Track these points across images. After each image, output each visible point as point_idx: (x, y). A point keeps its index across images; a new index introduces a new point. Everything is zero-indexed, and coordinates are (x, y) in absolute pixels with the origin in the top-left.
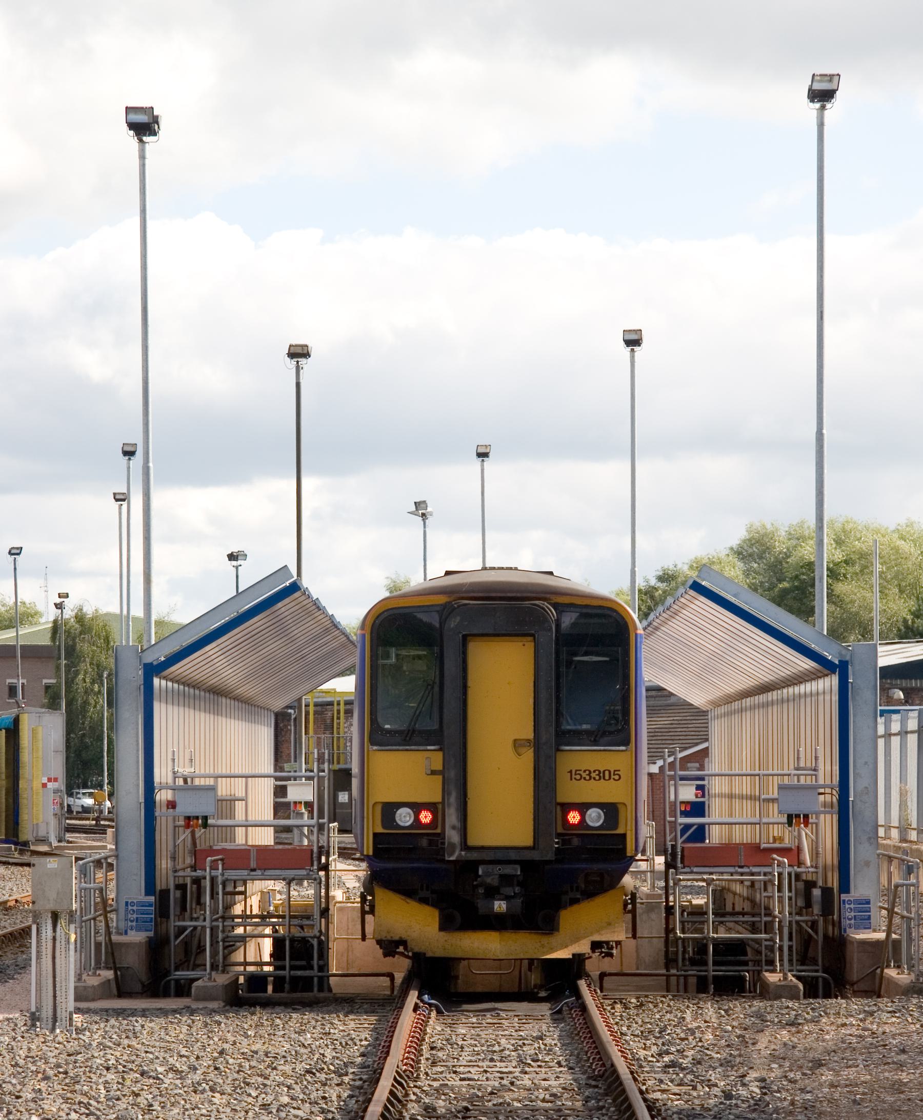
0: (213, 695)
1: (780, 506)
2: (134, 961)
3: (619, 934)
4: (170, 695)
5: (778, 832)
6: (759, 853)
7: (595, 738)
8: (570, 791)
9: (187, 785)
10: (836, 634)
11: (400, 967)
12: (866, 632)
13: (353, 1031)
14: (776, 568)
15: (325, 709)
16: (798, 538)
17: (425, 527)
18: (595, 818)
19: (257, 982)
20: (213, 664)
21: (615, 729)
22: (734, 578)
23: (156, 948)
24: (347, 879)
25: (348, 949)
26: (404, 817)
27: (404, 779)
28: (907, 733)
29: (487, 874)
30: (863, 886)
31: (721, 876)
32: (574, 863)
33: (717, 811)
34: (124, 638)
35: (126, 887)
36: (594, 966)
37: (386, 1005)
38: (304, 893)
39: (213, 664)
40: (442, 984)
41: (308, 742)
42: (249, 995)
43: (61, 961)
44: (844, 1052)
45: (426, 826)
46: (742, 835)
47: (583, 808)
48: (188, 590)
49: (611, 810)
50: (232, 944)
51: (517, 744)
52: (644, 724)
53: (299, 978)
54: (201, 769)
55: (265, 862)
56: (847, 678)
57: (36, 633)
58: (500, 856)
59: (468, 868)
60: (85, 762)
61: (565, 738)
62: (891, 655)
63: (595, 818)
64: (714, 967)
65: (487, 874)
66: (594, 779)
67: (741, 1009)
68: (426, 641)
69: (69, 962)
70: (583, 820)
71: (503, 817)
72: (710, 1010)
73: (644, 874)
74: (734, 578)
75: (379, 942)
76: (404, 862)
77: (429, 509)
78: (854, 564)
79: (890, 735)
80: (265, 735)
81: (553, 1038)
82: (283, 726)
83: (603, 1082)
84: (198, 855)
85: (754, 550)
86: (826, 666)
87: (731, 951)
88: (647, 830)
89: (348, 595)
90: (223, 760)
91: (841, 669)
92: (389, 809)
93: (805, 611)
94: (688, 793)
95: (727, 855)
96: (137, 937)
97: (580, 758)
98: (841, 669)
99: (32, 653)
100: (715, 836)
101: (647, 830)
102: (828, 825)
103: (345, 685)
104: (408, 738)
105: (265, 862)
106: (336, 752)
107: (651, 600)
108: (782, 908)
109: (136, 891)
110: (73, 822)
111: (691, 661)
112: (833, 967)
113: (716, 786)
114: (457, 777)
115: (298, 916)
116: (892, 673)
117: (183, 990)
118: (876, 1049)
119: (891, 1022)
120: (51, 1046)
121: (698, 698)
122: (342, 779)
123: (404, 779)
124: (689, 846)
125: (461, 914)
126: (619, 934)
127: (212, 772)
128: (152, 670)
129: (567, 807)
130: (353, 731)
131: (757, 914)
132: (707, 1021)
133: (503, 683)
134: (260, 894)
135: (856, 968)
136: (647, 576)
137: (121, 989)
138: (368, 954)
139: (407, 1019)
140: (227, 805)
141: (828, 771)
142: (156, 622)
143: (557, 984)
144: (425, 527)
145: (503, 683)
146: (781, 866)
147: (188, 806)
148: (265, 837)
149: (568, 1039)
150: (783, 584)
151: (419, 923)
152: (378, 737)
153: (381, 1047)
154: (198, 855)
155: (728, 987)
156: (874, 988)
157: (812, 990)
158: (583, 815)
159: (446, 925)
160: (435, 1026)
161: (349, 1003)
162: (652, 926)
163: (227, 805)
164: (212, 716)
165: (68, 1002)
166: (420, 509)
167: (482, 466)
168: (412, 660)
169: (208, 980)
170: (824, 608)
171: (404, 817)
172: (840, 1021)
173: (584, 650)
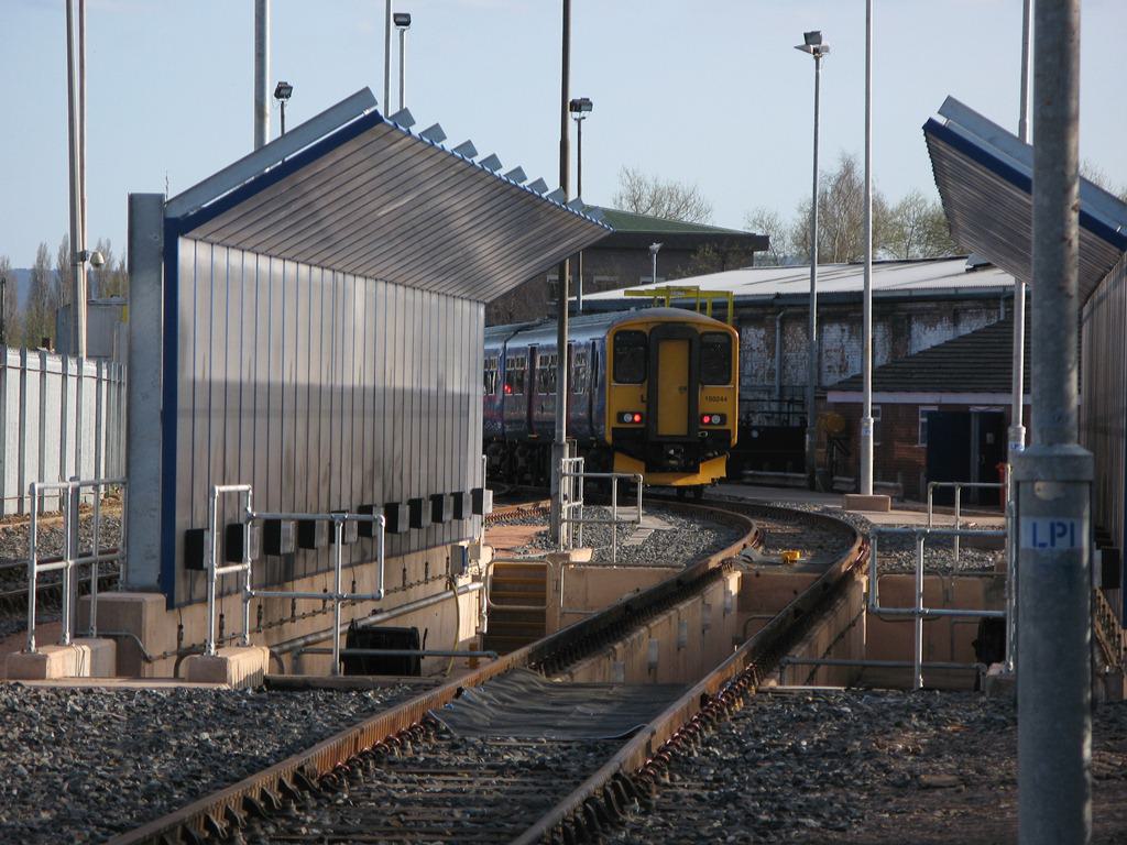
4: (303, 291)
8: (705, 406)
17: (817, 68)
45: (637, 423)
47: (711, 416)
51: (680, 389)
56: (1113, 231)
63: (716, 419)
70: (710, 420)
71: (672, 422)
75: (955, 325)
77: (823, 43)
114: (651, 402)
127: (450, 304)
129: (703, 415)
133: (673, 364)
142: (293, 673)
144: (817, 68)
145: (673, 364)
158: (711, 418)
164: (380, 385)
166: (812, 38)
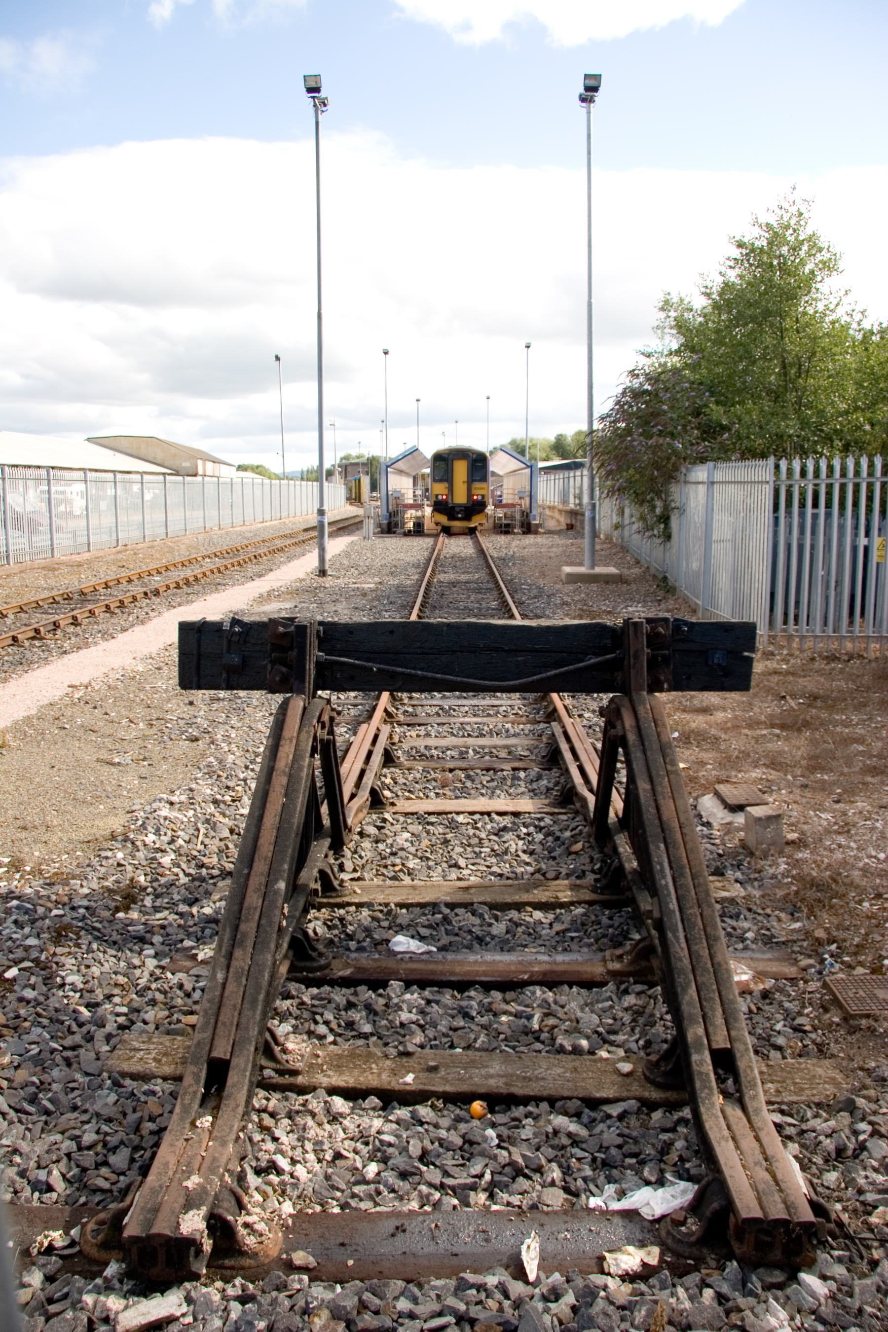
0: (401, 472)
1: (519, 434)
2: (385, 527)
3: (484, 521)
5: (517, 501)
6: (513, 505)
7: (480, 481)
8: (474, 492)
9: (395, 491)
10: (530, 460)
11: (439, 528)
12: (536, 460)
13: (430, 541)
14: (518, 447)
15: (423, 475)
16: (522, 440)
18: (480, 498)
19: (410, 531)
20: (400, 465)
21: (484, 479)
22: (509, 448)
23: (389, 524)
24: (428, 511)
25: (428, 525)
26: (440, 497)
27: (440, 489)
28: (713, 483)
29: (457, 509)
30: (534, 512)
31: (505, 510)
32: (476, 508)
33: (505, 496)
34: (382, 460)
35: (382, 512)
36: (479, 528)
37: (436, 536)
38: (419, 514)
39: (400, 465)
40: (447, 531)
41: (420, 482)
42: (408, 534)
43: (370, 526)
44: (530, 545)
46: (510, 502)
48: (394, 452)
49: (483, 496)
50: (404, 523)
52: (491, 479)
53: (418, 530)
54: (398, 488)
55: (411, 506)
57: (364, 460)
58: (460, 505)
59: (453, 508)
60: (374, 487)
61: (473, 481)
62: (541, 464)
64: (504, 529)
65: (457, 509)
66: (479, 491)
67: (509, 537)
68: (444, 462)
69: (372, 527)
71: (460, 497)
72: (503, 537)
73: (490, 509)
74: (509, 448)
76: (440, 507)
78: (534, 446)
79: (713, 483)
80: (411, 480)
81: (471, 543)
82: (415, 479)
83: (481, 552)
84: (397, 505)
85: (513, 442)
86: (528, 467)
87: (507, 525)
88: (491, 501)
89: (429, 452)
90: (402, 486)
91: (531, 467)
92: (437, 496)
93: (524, 455)
94: (499, 493)
95: (507, 506)
96: (385, 522)
97: (477, 485)
98: (531, 467)
99: (363, 464)
100: (504, 502)
101: (491, 501)
102: (528, 499)
103: (428, 471)
104: (441, 481)
105: (411, 506)
106: (426, 484)
107: (491, 453)
108: (518, 516)
109: (385, 513)
110: (372, 499)
111: (499, 465)
112: (528, 528)
113: (505, 491)
114: (451, 489)
115: (417, 518)
116: (541, 469)
117: (394, 533)
118: (536, 545)
119: (539, 539)
120: (368, 543)
121: (501, 473)
122: (427, 490)
123: (440, 489)
124: (499, 504)
125: (452, 517)
126: (484, 521)
128: (388, 467)
130: (429, 480)
131: (512, 518)
132: (502, 539)
133: (461, 469)
134: (411, 513)
135: (533, 529)
136: (491, 448)
137: (382, 532)
138: (433, 526)
139: (441, 539)
140: (403, 495)
141: (528, 488)
143: (472, 532)
145: (461, 469)
146: (518, 508)
147: (395, 495)
148: (411, 502)
149: (474, 543)
150: (519, 450)
151: (443, 519)
152: (435, 480)
153: (435, 544)
154: (397, 505)
155: (507, 533)
156: (536, 533)
157: (524, 533)
159: (449, 519)
160: (446, 541)
161: (429, 536)
162: (491, 521)
163: (403, 495)
165: (371, 534)
167: (589, 113)
168: (442, 464)
169: (399, 531)
170: (527, 455)
171: (440, 497)
172: (530, 539)
173: (478, 463)
